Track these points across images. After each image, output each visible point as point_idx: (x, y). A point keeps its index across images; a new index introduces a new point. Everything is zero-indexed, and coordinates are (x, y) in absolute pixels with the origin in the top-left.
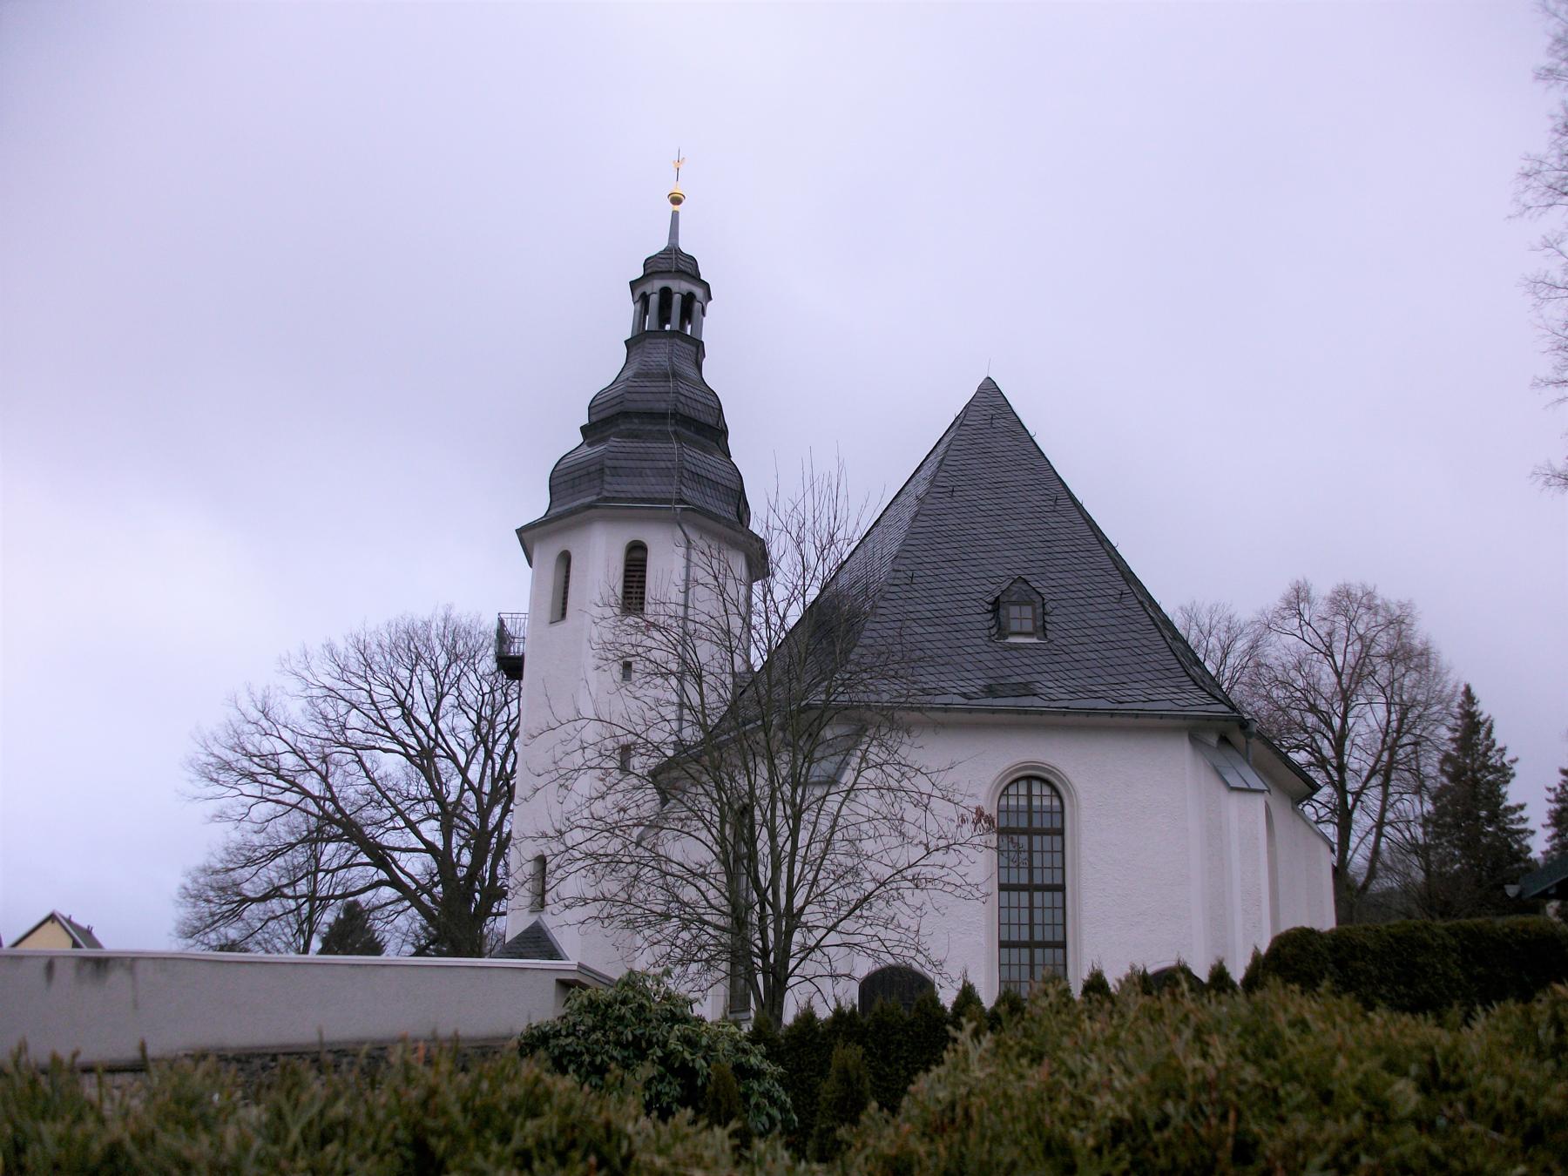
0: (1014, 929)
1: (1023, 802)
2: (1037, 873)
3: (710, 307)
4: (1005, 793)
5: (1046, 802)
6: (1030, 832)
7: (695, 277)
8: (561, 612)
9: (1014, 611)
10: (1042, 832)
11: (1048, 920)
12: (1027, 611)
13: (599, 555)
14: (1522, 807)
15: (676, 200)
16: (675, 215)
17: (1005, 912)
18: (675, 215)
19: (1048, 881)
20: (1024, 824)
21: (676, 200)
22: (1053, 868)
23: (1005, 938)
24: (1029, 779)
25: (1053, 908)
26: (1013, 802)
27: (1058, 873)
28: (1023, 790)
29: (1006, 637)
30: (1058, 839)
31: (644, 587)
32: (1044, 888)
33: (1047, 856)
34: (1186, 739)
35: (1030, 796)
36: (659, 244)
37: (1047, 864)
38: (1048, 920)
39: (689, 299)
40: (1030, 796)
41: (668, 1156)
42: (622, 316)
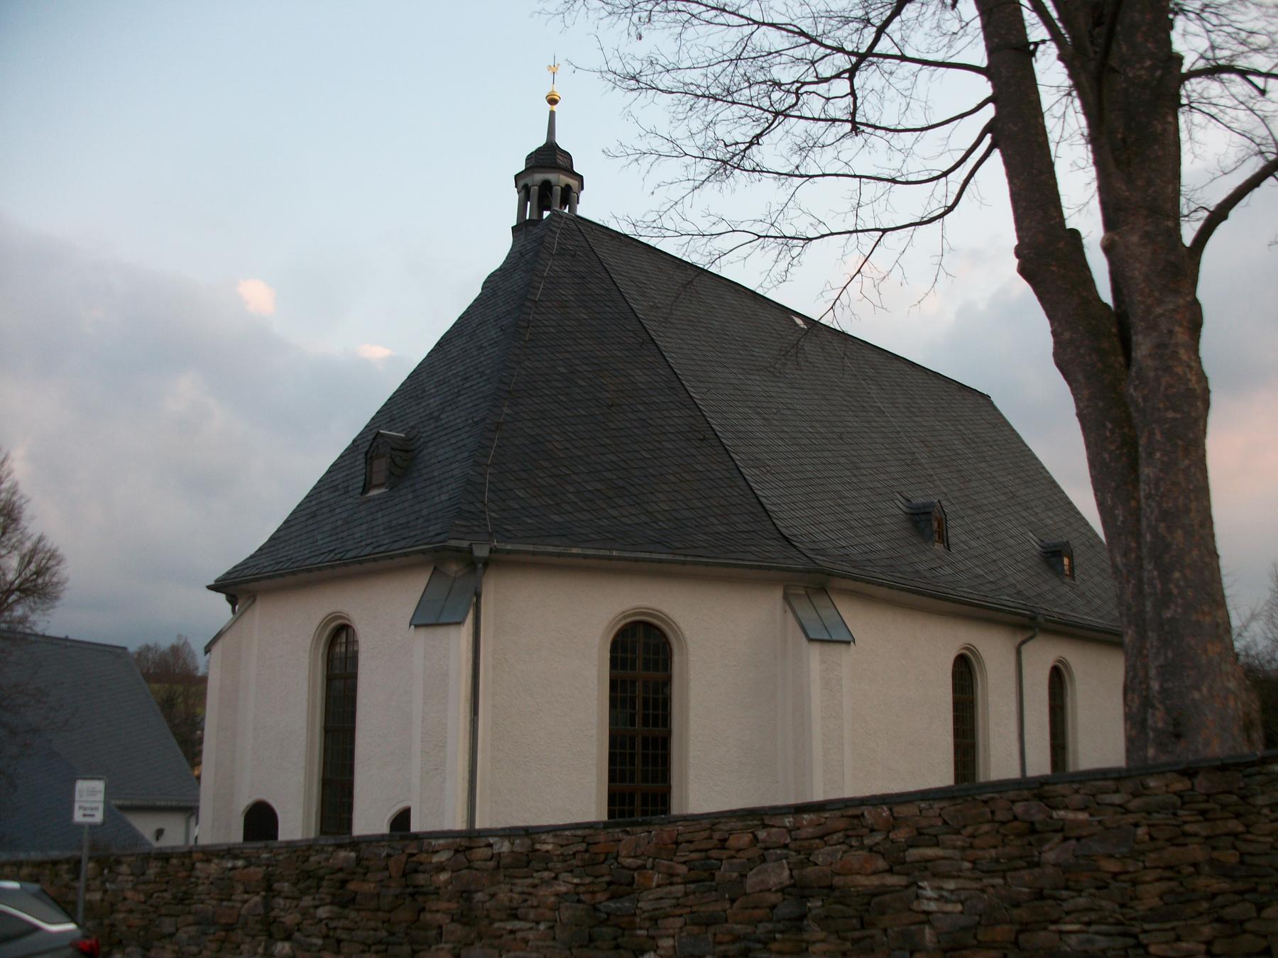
3: (583, 195)
7: (569, 170)
15: (553, 101)
16: (552, 114)
18: (552, 114)
21: (553, 101)
31: (1079, 513)
34: (778, 594)
36: (541, 141)
39: (567, 190)
41: (358, 852)
42: (505, 208)
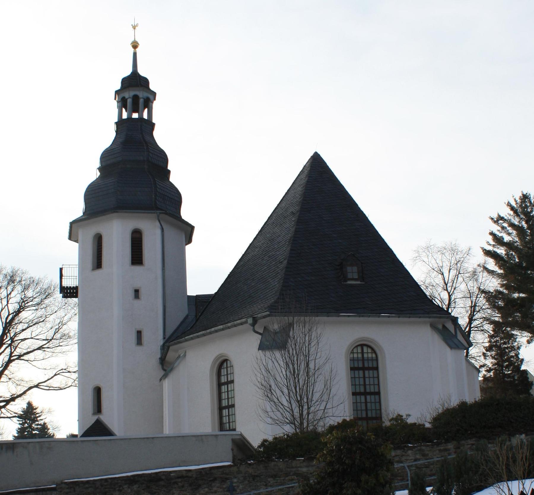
0: (357, 387)
1: (360, 356)
2: (368, 387)
4: (352, 352)
5: (370, 355)
6: (364, 369)
8: (98, 264)
9: (349, 269)
10: (369, 369)
11: (372, 383)
12: (355, 269)
13: (116, 232)
14: (509, 204)
15: (134, 27)
16: (135, 55)
17: (356, 412)
18: (135, 55)
19: (372, 390)
20: (361, 365)
22: (374, 377)
23: (352, 366)
24: (362, 346)
25: (375, 402)
26: (355, 355)
27: (376, 387)
28: (359, 350)
29: (346, 281)
30: (375, 372)
32: (371, 394)
33: (372, 380)
35: (363, 353)
36: (128, 72)
37: (372, 383)
38: (374, 408)
40: (363, 353)
